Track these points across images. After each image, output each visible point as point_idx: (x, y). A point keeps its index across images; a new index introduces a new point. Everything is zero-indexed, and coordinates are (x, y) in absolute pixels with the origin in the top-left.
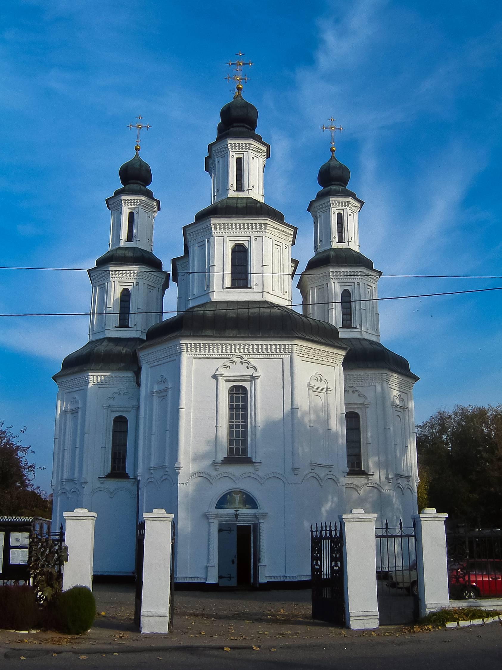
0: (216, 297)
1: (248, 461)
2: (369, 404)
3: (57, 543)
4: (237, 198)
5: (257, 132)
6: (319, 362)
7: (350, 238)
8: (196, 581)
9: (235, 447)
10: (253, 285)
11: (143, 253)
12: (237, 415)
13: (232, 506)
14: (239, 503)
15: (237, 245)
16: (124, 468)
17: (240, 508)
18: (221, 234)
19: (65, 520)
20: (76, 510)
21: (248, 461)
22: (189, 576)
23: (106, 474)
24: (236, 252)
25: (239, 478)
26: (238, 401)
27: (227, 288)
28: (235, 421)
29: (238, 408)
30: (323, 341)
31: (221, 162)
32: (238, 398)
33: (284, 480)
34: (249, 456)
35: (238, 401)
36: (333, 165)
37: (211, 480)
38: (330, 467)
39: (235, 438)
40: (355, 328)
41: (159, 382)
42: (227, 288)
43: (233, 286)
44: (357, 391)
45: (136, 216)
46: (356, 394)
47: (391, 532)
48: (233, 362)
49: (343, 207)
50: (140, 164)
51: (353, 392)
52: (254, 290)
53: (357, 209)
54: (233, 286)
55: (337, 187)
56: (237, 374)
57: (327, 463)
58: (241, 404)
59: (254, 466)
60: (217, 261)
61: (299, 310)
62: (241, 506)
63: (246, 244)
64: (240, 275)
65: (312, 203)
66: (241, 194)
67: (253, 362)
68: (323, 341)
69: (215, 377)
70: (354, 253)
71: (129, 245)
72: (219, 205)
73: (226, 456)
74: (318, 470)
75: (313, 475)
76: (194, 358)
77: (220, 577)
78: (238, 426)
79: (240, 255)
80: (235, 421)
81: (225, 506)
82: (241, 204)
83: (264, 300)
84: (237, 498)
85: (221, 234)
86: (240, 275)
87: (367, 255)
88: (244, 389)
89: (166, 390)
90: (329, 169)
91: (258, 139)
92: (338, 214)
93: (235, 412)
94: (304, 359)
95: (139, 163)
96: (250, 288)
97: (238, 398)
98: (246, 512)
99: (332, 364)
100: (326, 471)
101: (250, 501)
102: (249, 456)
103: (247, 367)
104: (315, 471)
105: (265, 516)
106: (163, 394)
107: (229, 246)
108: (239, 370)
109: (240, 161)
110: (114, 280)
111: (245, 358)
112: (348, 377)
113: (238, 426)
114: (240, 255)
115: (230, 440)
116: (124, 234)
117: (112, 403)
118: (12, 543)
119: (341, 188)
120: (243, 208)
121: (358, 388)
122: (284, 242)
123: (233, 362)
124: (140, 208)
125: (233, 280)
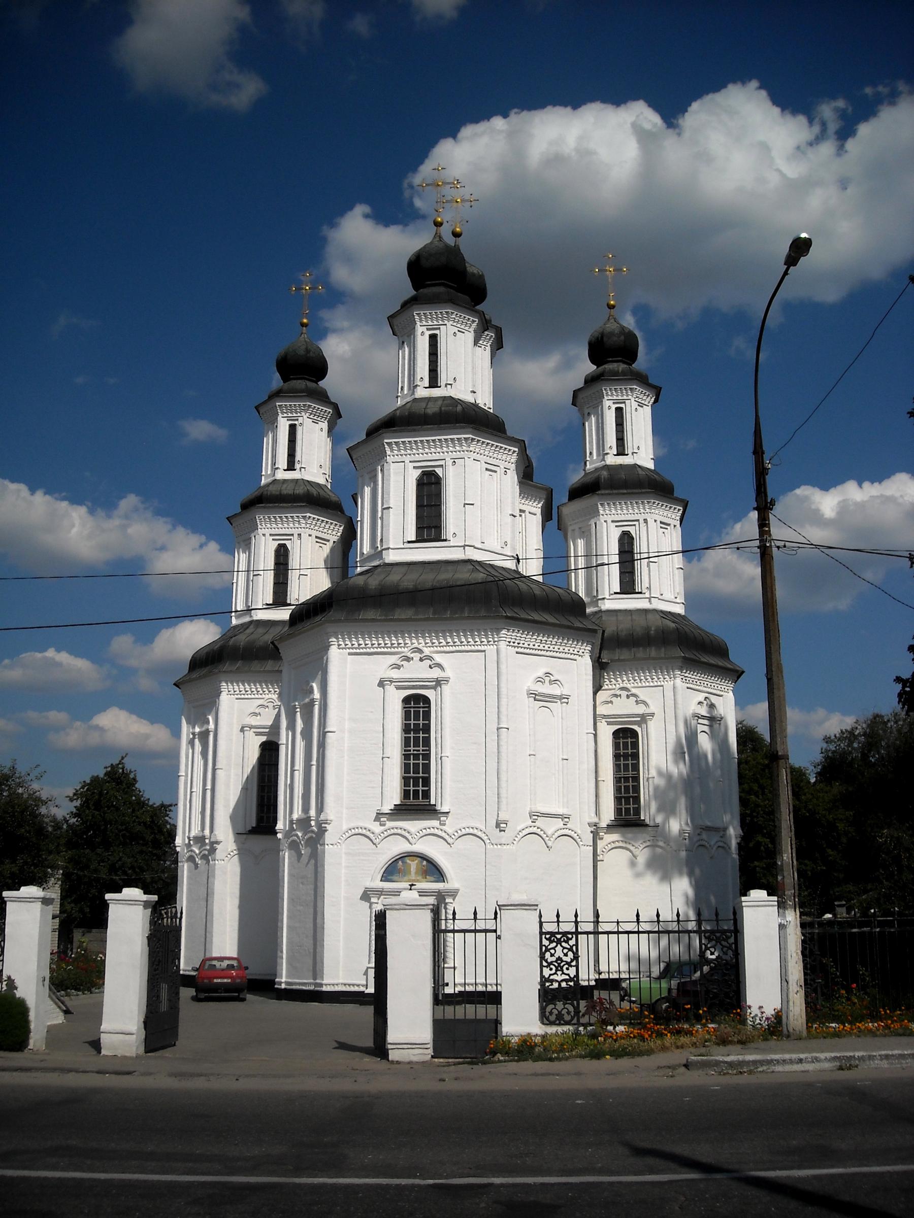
0: (392, 557)
2: (653, 715)
3: (570, 936)
4: (429, 399)
6: (548, 654)
7: (635, 447)
8: (352, 989)
9: (412, 788)
10: (449, 536)
11: (309, 488)
12: (416, 739)
13: (406, 878)
14: (416, 873)
15: (424, 474)
17: (418, 881)
18: (399, 459)
19: (5, 903)
20: (23, 889)
22: (341, 981)
24: (424, 484)
25: (416, 836)
26: (417, 718)
27: (409, 542)
28: (412, 748)
29: (417, 729)
30: (551, 619)
32: (417, 714)
33: (485, 838)
34: (433, 802)
35: (417, 718)
36: (608, 330)
37: (410, 837)
38: (564, 817)
39: (412, 775)
40: (641, 593)
42: (409, 542)
43: (421, 538)
44: (634, 695)
45: (299, 430)
46: (633, 699)
48: (408, 659)
49: (625, 397)
50: (307, 349)
51: (628, 697)
52: (452, 544)
54: (421, 538)
55: (615, 365)
56: (420, 676)
57: (560, 811)
58: (421, 722)
59: (439, 819)
60: (394, 500)
61: (533, 568)
62: (419, 878)
63: (439, 471)
64: (430, 524)
65: (576, 393)
66: (436, 393)
67: (438, 658)
68: (551, 619)
69: (381, 684)
70: (640, 472)
71: (290, 475)
72: (398, 412)
73: (398, 802)
74: (541, 822)
75: (535, 830)
76: (350, 654)
78: (416, 757)
79: (430, 489)
80: (412, 748)
81: (394, 878)
82: (432, 409)
83: (467, 558)
84: (413, 864)
85: (399, 459)
86: (430, 524)
87: (668, 476)
88: (426, 700)
90: (602, 337)
92: (617, 409)
93: (412, 735)
94: (520, 650)
95: (304, 347)
96: (446, 540)
97: (417, 714)
99: (572, 657)
100: (559, 823)
102: (433, 802)
103: (430, 667)
104: (537, 824)
105: (454, 894)
107: (413, 475)
108: (417, 671)
109: (433, 339)
110: (263, 531)
111: (427, 651)
113: (416, 757)
114: (430, 489)
115: (404, 778)
116: (282, 461)
120: (434, 414)
121: (634, 691)
122: (503, 465)
123: (408, 659)
124: (305, 417)
125: (419, 529)
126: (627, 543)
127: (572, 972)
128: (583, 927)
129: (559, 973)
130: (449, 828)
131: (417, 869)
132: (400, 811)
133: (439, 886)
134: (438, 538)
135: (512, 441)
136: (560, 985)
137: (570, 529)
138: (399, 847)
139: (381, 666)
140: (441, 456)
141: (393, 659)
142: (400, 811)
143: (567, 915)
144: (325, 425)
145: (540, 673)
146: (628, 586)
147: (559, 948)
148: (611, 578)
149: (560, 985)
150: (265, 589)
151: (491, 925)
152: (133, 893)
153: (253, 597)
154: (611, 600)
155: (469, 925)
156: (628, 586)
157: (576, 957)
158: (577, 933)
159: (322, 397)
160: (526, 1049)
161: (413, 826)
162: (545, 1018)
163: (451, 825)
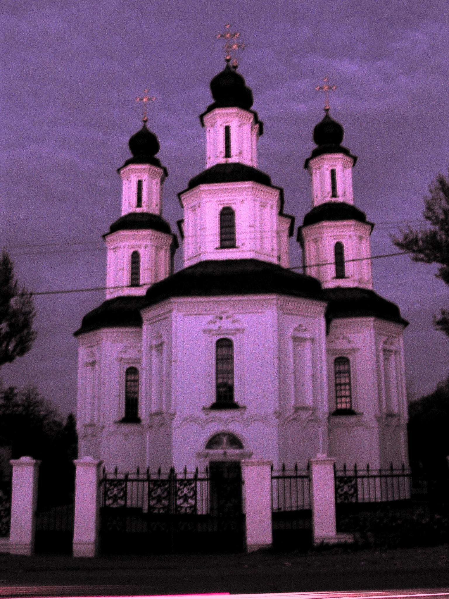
1: (235, 406)
5: (343, 144)
16: (136, 413)
21: (235, 406)
23: (121, 418)
25: (226, 421)
31: (211, 132)
41: (156, 337)
46: (230, 320)
47: (299, 473)
53: (351, 165)
54: (222, 247)
77: (212, 509)
79: (227, 216)
84: (225, 439)
87: (361, 208)
89: (161, 344)
91: (346, 152)
98: (233, 453)
101: (235, 441)
106: (160, 347)
107: (334, 242)
108: (226, 324)
112: (232, 303)
114: (227, 216)
117: (124, 356)
118: (401, 479)
119: (334, 145)
126: (339, 249)
127: (191, 502)
128: (360, 473)
129: (186, 503)
130: (246, 416)
131: (227, 441)
132: (215, 407)
133: (238, 451)
134: (233, 246)
135: (276, 188)
136: (186, 510)
137: (306, 240)
138: (213, 428)
139: (203, 321)
140: (234, 198)
141: (210, 318)
142: (215, 407)
143: (350, 467)
144: (159, 180)
145: (297, 325)
146: (340, 274)
147: (346, 487)
148: (330, 271)
149: (186, 510)
150: (125, 278)
151: (304, 473)
152: (25, 459)
153: (116, 281)
154: (330, 282)
155: (293, 473)
156: (340, 274)
157: (195, 493)
158: (356, 477)
159: (156, 163)
160: (325, 547)
161: (225, 414)
162: (340, 528)
163: (247, 414)
